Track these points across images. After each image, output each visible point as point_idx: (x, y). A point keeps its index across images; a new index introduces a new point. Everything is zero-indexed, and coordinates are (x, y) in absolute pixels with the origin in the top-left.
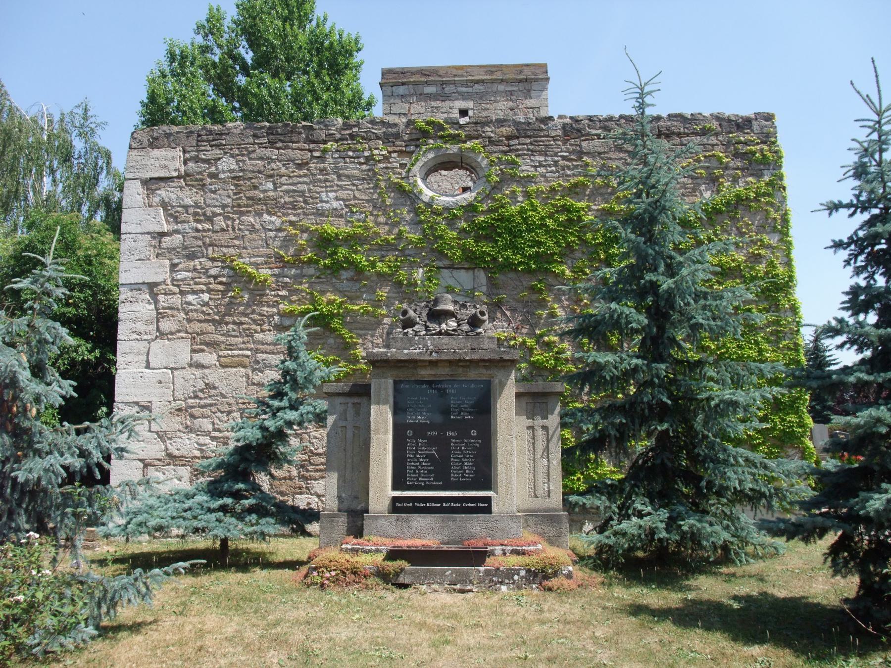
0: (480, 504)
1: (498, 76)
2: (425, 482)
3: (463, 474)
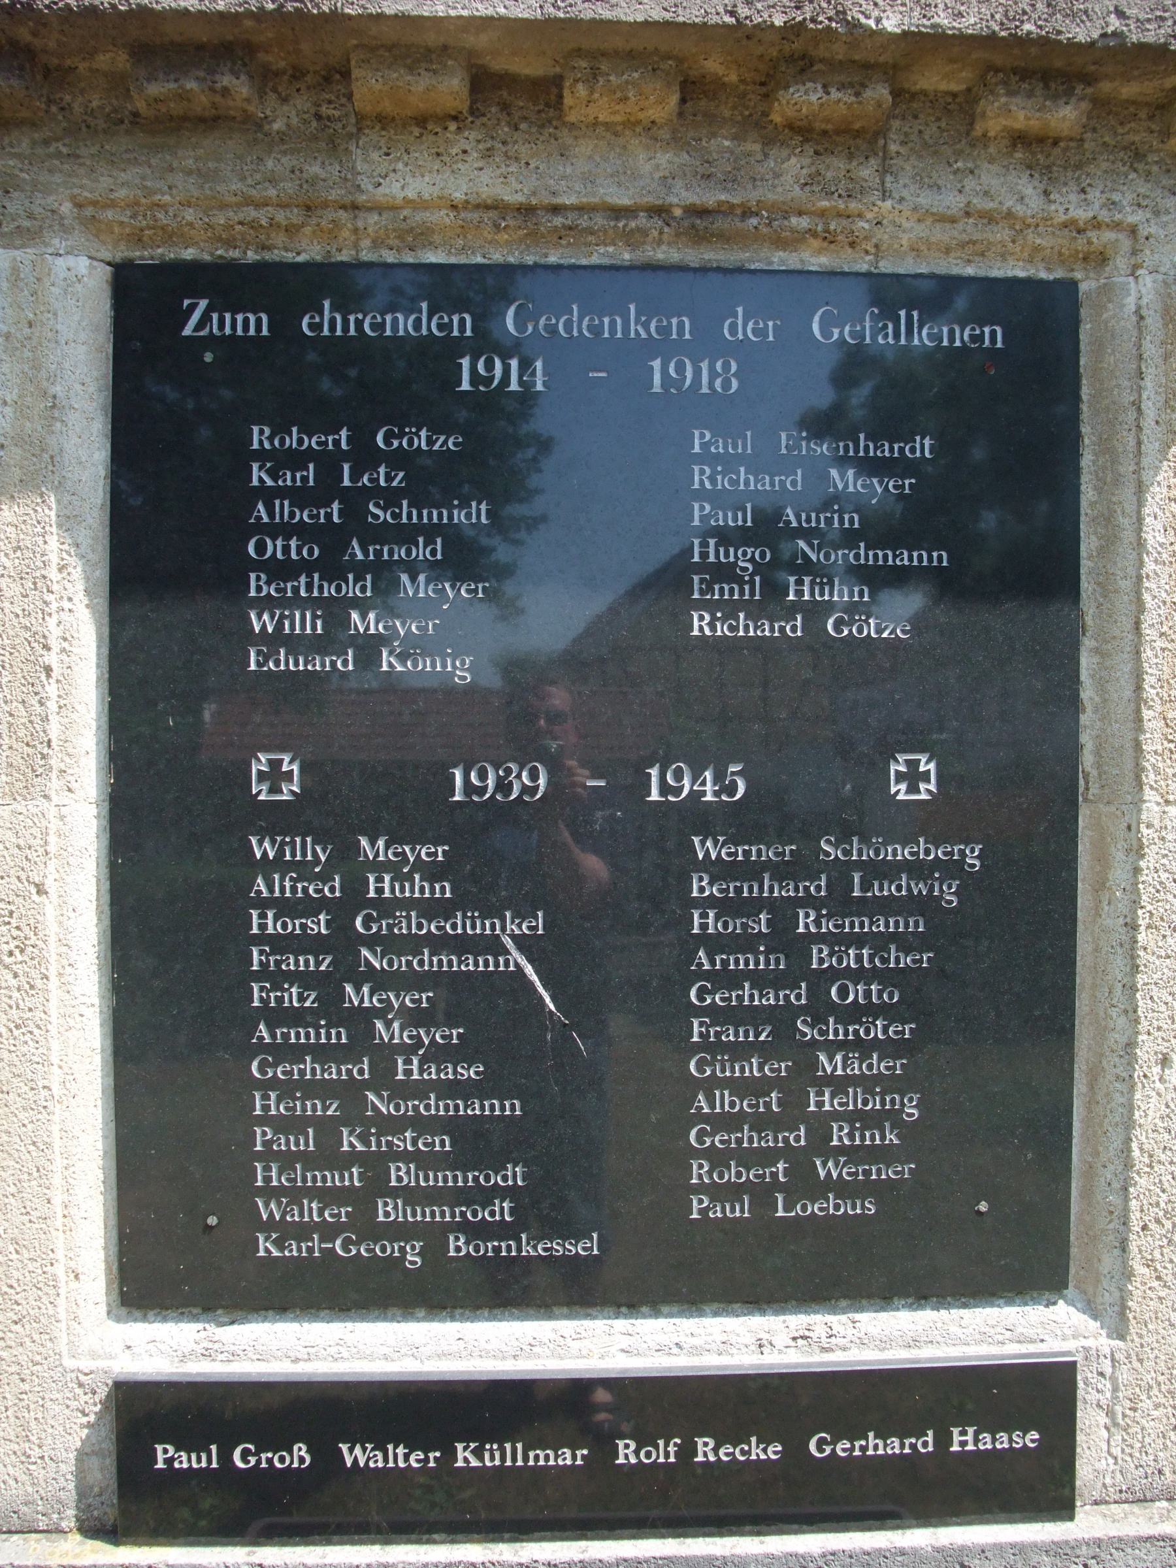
0: (963, 1440)
1: (618, 43)
2: (434, 1236)
3: (800, 1163)
